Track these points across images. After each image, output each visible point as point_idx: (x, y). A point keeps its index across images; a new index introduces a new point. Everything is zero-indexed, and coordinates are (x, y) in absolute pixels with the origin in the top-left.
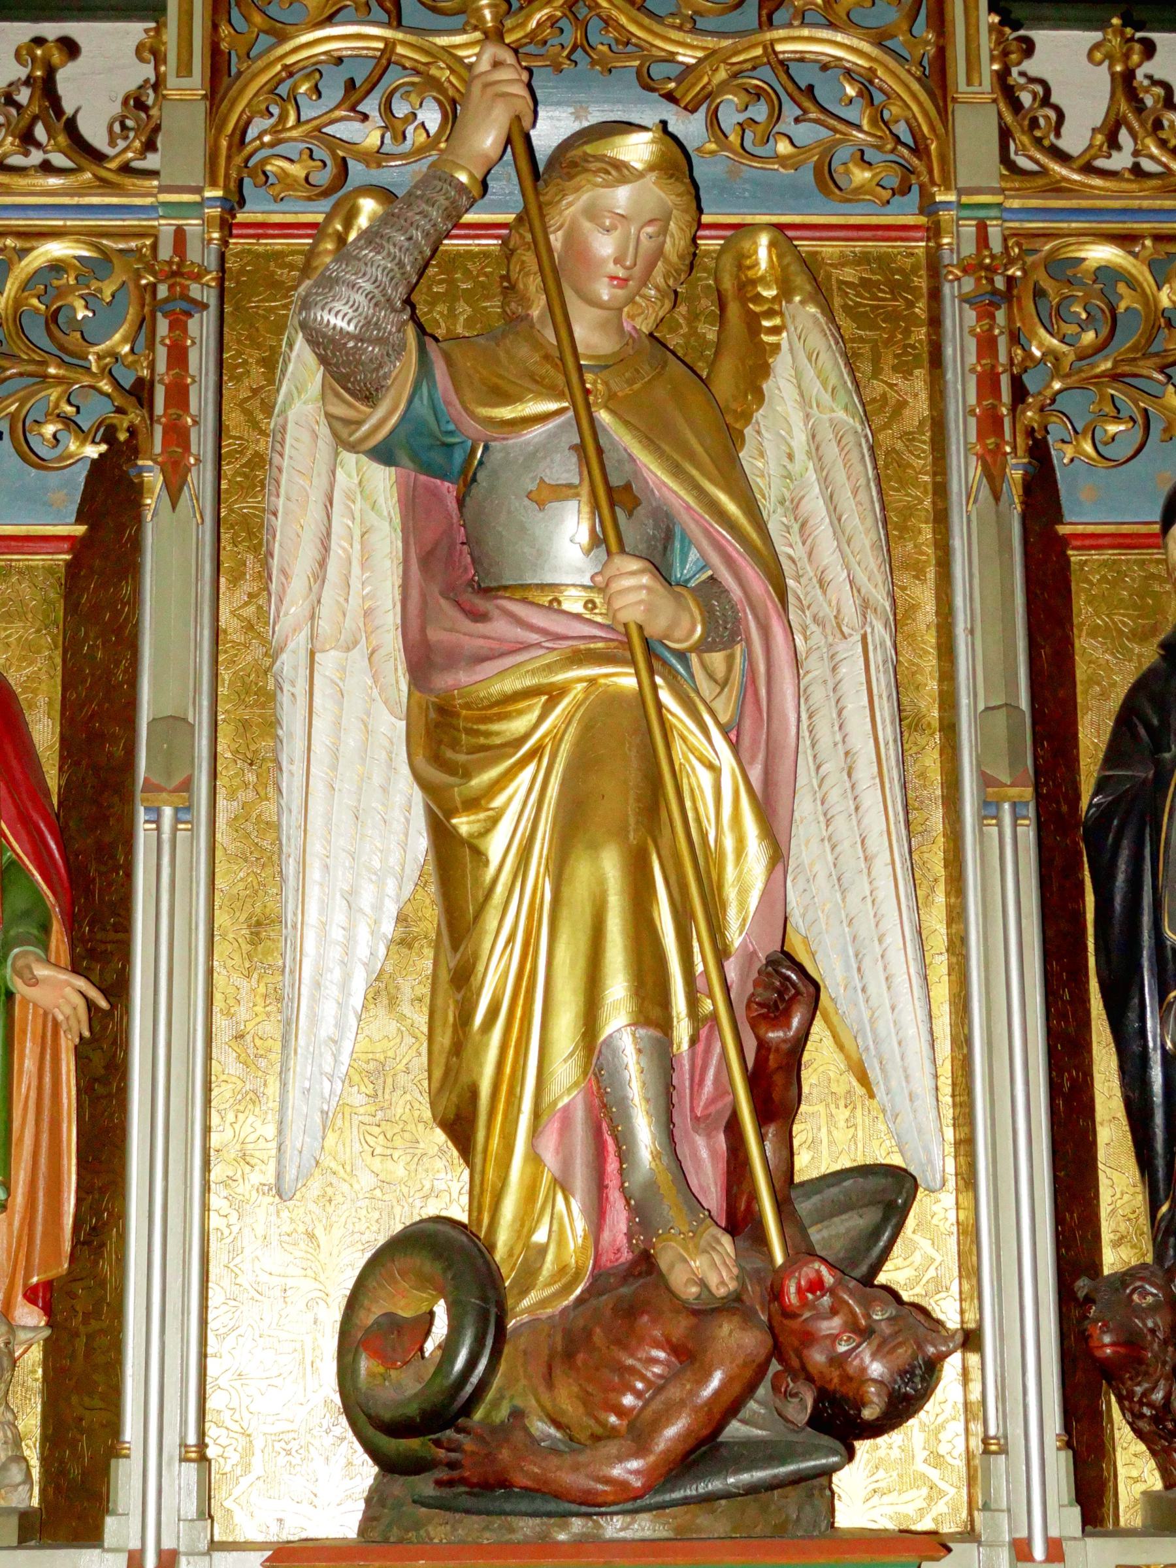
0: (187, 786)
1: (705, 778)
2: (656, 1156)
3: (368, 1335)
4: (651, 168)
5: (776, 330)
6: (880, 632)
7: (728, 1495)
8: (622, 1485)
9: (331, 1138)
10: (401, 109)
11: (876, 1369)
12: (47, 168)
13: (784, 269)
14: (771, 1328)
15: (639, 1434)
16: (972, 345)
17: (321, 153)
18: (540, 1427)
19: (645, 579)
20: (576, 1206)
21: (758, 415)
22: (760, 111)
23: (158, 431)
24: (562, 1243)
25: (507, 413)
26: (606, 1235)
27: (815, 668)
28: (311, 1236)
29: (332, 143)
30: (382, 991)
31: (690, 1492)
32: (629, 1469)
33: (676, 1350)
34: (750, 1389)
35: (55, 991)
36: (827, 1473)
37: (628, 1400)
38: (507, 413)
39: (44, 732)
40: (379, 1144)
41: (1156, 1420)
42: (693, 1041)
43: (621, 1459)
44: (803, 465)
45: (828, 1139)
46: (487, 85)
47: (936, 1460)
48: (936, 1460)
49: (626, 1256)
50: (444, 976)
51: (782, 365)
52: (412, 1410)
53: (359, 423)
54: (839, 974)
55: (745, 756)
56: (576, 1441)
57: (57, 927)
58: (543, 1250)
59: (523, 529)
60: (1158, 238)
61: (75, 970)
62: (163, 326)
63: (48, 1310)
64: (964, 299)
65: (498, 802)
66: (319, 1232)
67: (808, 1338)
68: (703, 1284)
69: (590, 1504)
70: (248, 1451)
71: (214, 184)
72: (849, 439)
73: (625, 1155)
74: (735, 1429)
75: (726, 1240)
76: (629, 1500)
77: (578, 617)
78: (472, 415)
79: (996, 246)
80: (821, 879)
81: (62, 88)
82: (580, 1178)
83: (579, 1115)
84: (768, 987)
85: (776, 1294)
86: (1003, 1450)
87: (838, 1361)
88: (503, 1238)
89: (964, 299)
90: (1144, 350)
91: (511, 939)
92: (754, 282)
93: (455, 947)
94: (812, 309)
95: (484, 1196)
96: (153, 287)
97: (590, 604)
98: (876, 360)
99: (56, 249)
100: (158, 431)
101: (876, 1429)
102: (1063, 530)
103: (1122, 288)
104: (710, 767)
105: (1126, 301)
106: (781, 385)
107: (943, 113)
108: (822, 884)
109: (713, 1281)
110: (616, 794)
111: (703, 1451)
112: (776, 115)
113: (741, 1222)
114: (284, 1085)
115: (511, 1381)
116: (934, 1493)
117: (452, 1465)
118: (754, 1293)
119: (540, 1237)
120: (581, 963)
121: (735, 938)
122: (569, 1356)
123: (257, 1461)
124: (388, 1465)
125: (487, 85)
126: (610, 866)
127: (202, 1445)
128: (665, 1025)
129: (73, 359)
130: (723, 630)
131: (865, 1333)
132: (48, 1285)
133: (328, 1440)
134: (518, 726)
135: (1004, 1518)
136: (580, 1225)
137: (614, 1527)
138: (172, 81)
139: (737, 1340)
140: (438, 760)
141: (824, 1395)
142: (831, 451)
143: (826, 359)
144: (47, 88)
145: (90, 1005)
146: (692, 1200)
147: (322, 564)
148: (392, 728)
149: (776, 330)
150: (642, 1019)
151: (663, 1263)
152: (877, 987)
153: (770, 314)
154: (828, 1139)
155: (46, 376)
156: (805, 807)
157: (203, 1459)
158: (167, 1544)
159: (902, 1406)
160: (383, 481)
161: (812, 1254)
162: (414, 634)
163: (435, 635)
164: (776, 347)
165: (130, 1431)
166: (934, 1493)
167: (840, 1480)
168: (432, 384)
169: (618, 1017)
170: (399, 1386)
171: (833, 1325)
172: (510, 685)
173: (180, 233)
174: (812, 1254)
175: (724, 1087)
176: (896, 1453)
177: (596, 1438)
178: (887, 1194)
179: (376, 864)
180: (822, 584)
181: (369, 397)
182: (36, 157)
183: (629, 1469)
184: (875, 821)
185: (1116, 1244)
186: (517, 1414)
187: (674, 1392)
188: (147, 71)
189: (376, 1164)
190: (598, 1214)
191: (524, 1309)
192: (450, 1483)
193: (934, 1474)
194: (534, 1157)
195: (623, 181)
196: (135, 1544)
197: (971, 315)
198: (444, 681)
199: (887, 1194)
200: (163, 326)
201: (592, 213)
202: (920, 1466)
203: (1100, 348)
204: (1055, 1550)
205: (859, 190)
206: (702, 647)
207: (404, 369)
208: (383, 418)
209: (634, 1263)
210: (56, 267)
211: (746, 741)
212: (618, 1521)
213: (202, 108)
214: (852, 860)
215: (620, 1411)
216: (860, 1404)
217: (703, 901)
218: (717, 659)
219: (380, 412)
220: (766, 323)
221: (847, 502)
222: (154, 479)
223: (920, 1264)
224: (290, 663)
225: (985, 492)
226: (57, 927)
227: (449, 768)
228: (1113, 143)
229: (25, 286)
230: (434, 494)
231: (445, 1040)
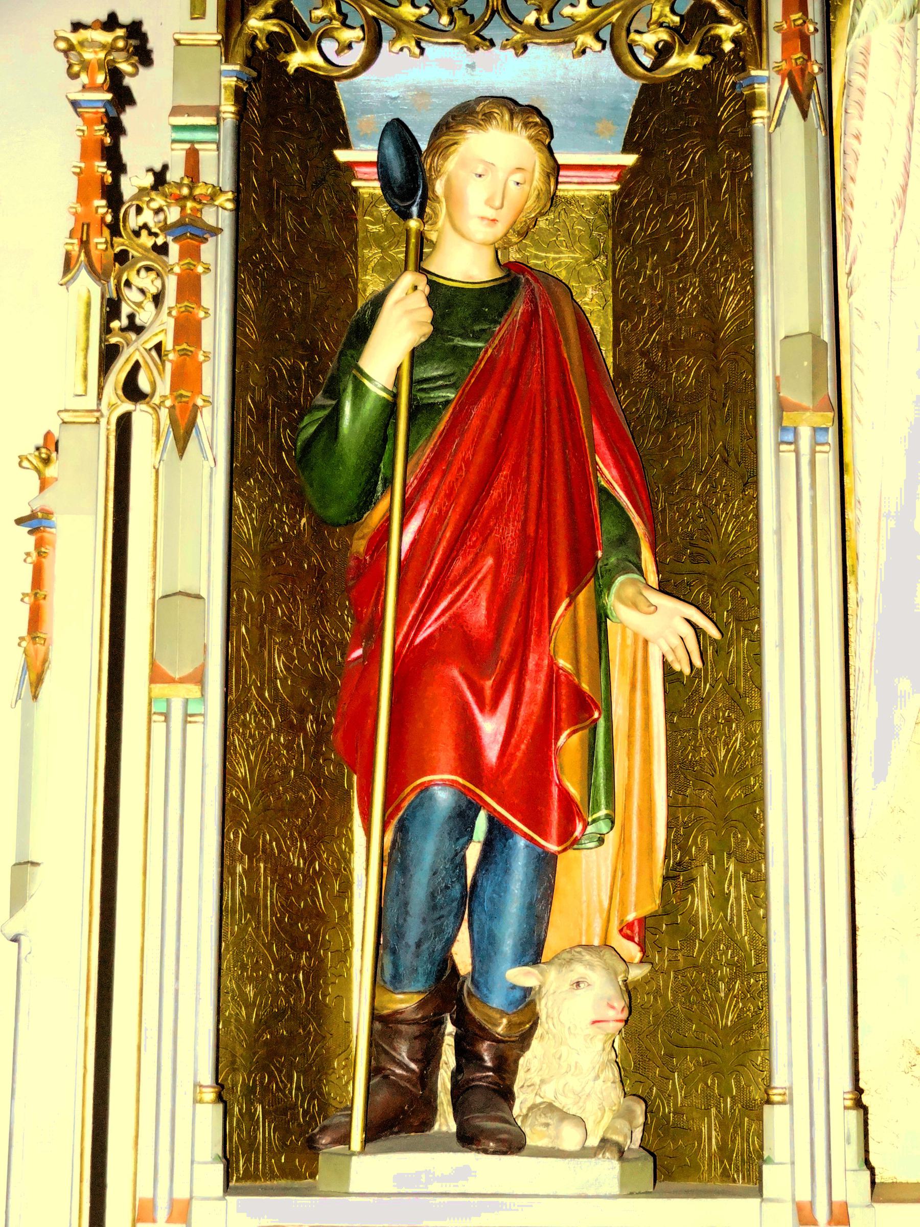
35: (653, 625)
196: (804, 1196)
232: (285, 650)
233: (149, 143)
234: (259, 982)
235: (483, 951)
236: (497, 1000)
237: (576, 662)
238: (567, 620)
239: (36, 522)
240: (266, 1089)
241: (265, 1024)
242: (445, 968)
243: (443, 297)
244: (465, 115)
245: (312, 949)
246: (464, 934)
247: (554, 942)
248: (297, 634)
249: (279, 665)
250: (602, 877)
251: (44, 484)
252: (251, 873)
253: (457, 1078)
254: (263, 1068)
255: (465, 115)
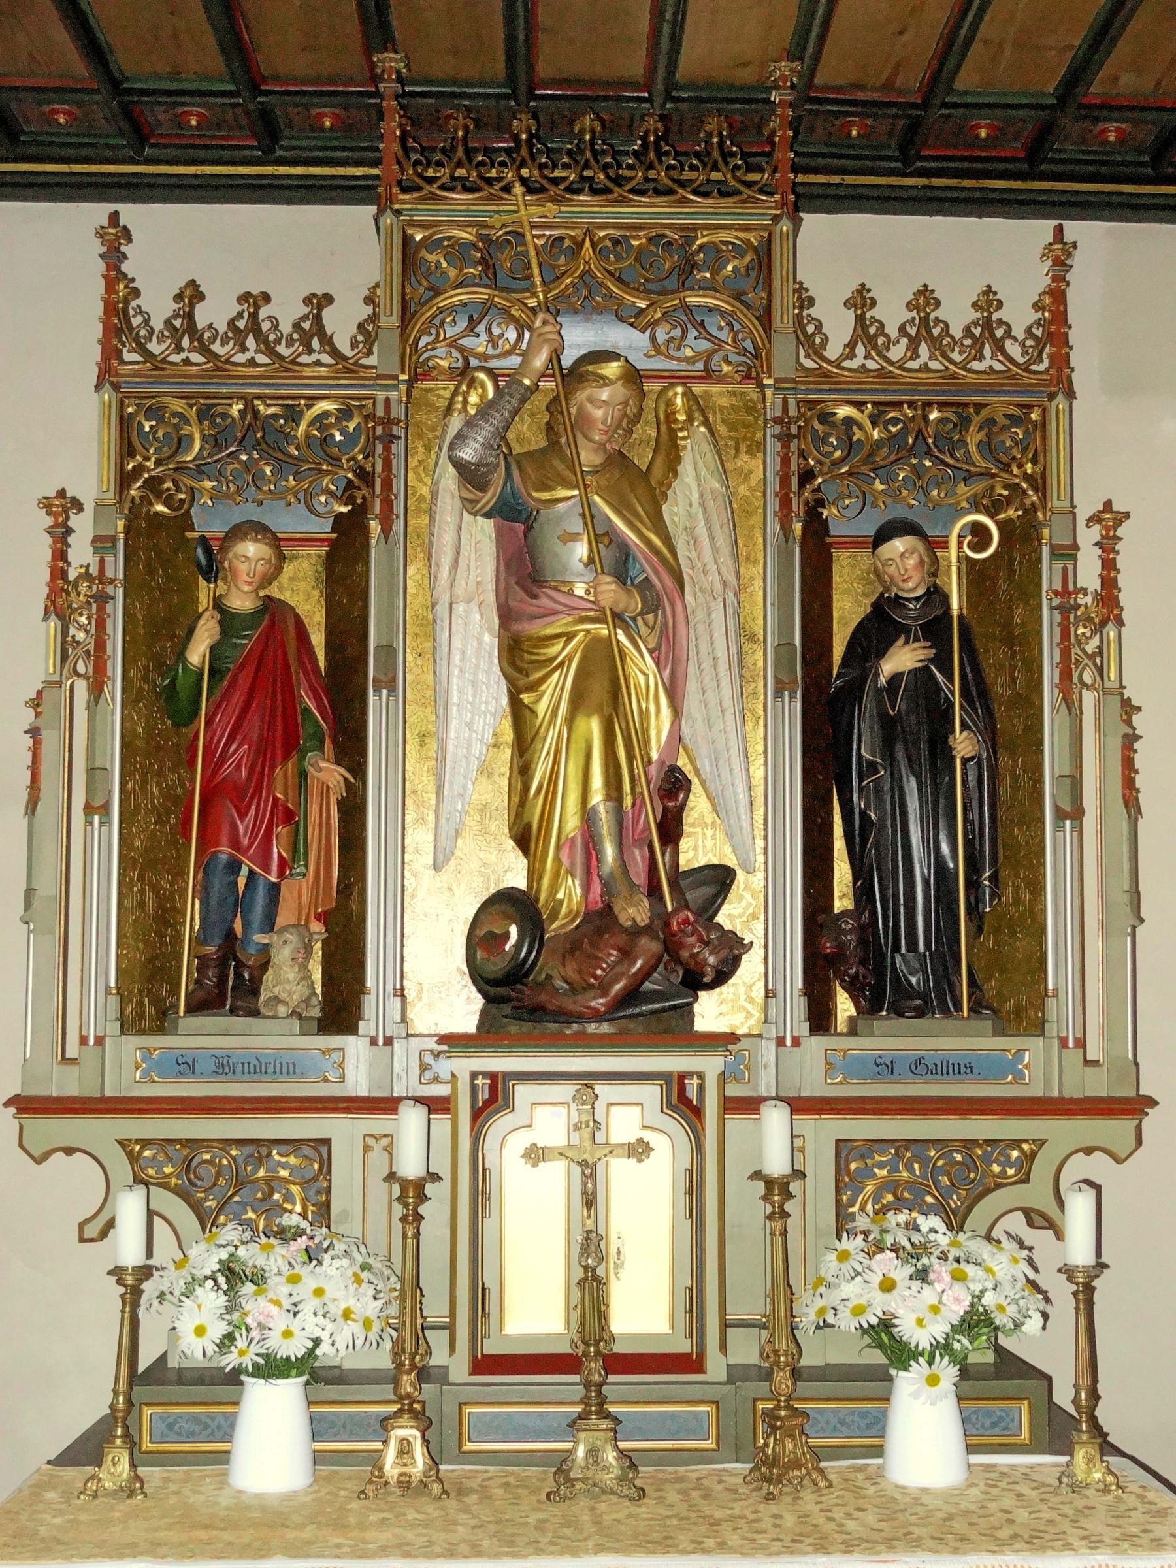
0: (394, 680)
1: (642, 678)
2: (615, 860)
3: (480, 940)
4: (618, 379)
5: (684, 438)
6: (731, 597)
7: (642, 1014)
8: (596, 1010)
9: (460, 841)
10: (496, 331)
11: (712, 960)
12: (318, 363)
13: (690, 407)
14: (665, 943)
15: (604, 989)
16: (778, 459)
17: (456, 354)
18: (559, 983)
19: (613, 586)
20: (577, 883)
21: (676, 483)
22: (677, 332)
23: (378, 502)
24: (570, 899)
25: (546, 496)
26: (591, 896)
27: (701, 615)
28: (450, 889)
29: (461, 350)
30: (485, 770)
31: (631, 1011)
32: (599, 1003)
33: (620, 950)
34: (653, 969)
35: (328, 773)
36: (691, 1005)
37: (599, 972)
38: (546, 496)
39: (318, 639)
40: (483, 845)
41: (851, 983)
42: (634, 805)
43: (595, 998)
44: (696, 509)
45: (699, 848)
46: (540, 335)
47: (750, 999)
48: (750, 999)
49: (600, 905)
50: (516, 768)
51: (687, 456)
52: (500, 975)
53: (477, 502)
54: (708, 769)
55: (662, 665)
56: (574, 989)
57: (328, 742)
58: (561, 902)
59: (556, 555)
60: (874, 404)
61: (338, 763)
62: (379, 448)
63: (326, 924)
64: (775, 437)
65: (543, 687)
66: (454, 887)
67: (680, 945)
68: (634, 920)
69: (581, 1018)
70: (421, 991)
71: (403, 372)
72: (720, 498)
73: (599, 854)
74: (647, 986)
75: (646, 901)
76: (597, 1017)
77: (581, 598)
78: (530, 495)
79: (793, 411)
80: (700, 720)
81: (325, 321)
82: (579, 869)
83: (579, 841)
84: (670, 783)
85: (667, 924)
86: (775, 996)
87: (693, 956)
88: (543, 896)
89: (775, 437)
90: (865, 461)
91: (548, 754)
92: (674, 413)
93: (521, 756)
94: (702, 429)
95: (534, 875)
96: (374, 428)
97: (588, 592)
98: (737, 450)
99: (325, 406)
100: (378, 502)
101: (710, 987)
102: (829, 540)
103: (855, 429)
104: (644, 673)
105: (858, 435)
106: (686, 468)
107: (769, 337)
108: (700, 724)
109: (638, 919)
110: (599, 689)
111: (632, 996)
112: (685, 333)
113: (654, 891)
114: (437, 816)
115: (545, 963)
116: (749, 1015)
117: (518, 1000)
118: (658, 924)
119: (560, 896)
120: (580, 774)
121: (655, 756)
122: (572, 952)
123: (425, 996)
124: (490, 999)
125: (540, 335)
126: (594, 727)
127: (402, 989)
128: (619, 800)
129: (335, 461)
130: (652, 605)
131: (707, 944)
132: (325, 913)
133: (459, 987)
134: (552, 651)
135: (773, 1027)
136: (579, 891)
137: (592, 1028)
138: (382, 318)
139: (649, 946)
140: (513, 664)
141: (687, 972)
142: (711, 504)
143: (709, 456)
144: (318, 319)
145: (346, 779)
146: (631, 884)
147: (456, 560)
148: (490, 641)
149: (684, 438)
150: (608, 798)
151: (616, 910)
152: (725, 771)
153: (682, 429)
154: (699, 848)
155: (320, 470)
156: (692, 685)
157: (403, 996)
158: (388, 1034)
159: (722, 977)
160: (487, 526)
161: (687, 907)
162: (502, 599)
163: (512, 603)
164: (685, 447)
165: (370, 983)
166: (749, 1015)
167: (697, 1008)
168: (512, 481)
169: (597, 797)
170: (494, 964)
171: (691, 940)
172: (549, 631)
173: (387, 400)
174: (687, 907)
175: (647, 827)
176: (731, 996)
177: (584, 989)
178: (720, 879)
179: (483, 707)
180: (705, 572)
181: (482, 487)
182: (314, 357)
183: (599, 1003)
184: (726, 691)
185: (841, 898)
186: (549, 977)
187: (619, 969)
188: (370, 310)
189: (482, 855)
190: (587, 886)
191: (553, 928)
192: (519, 1008)
193: (749, 1007)
194: (557, 859)
195: (606, 385)
196: (373, 1033)
197: (779, 445)
198: (516, 627)
199: (720, 879)
200: (379, 448)
201: (590, 400)
202: (742, 1002)
203: (842, 460)
204: (796, 1042)
205: (726, 375)
206: (641, 614)
207: (499, 477)
208: (489, 498)
209: (603, 909)
210: (325, 414)
211: (662, 658)
212: (593, 1026)
213: (398, 332)
214: (715, 712)
215: (596, 977)
216: (703, 975)
217: (637, 741)
218: (650, 617)
219: (489, 494)
220: (680, 434)
221: (716, 528)
222: (375, 526)
223: (733, 914)
224: (442, 610)
225: (782, 537)
226: (328, 742)
227: (520, 670)
228: (852, 356)
229: (311, 424)
230: (511, 529)
231: (516, 799)
232: (159, 784)
233: (81, 554)
234: (146, 942)
235: (246, 924)
236: (252, 950)
237: (285, 794)
238: (282, 778)
239: (34, 732)
240: (150, 991)
241: (151, 960)
242: (230, 935)
243: (228, 619)
244: (238, 532)
245: (173, 926)
246: (239, 919)
247: (280, 921)
248: (166, 777)
249: (156, 791)
250: (298, 895)
251: (37, 715)
252: (142, 892)
253: (231, 985)
254: (149, 981)
255: (238, 532)
